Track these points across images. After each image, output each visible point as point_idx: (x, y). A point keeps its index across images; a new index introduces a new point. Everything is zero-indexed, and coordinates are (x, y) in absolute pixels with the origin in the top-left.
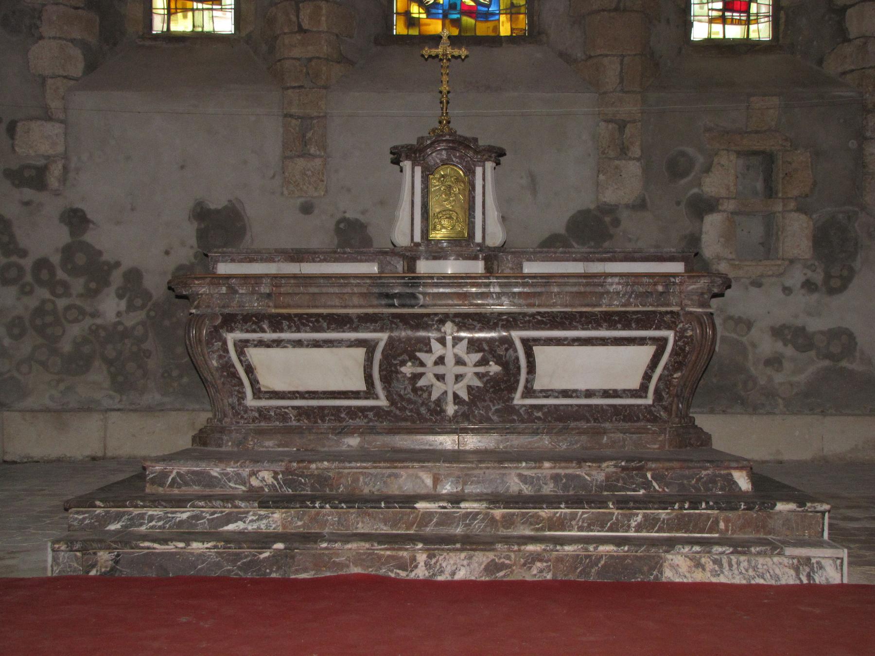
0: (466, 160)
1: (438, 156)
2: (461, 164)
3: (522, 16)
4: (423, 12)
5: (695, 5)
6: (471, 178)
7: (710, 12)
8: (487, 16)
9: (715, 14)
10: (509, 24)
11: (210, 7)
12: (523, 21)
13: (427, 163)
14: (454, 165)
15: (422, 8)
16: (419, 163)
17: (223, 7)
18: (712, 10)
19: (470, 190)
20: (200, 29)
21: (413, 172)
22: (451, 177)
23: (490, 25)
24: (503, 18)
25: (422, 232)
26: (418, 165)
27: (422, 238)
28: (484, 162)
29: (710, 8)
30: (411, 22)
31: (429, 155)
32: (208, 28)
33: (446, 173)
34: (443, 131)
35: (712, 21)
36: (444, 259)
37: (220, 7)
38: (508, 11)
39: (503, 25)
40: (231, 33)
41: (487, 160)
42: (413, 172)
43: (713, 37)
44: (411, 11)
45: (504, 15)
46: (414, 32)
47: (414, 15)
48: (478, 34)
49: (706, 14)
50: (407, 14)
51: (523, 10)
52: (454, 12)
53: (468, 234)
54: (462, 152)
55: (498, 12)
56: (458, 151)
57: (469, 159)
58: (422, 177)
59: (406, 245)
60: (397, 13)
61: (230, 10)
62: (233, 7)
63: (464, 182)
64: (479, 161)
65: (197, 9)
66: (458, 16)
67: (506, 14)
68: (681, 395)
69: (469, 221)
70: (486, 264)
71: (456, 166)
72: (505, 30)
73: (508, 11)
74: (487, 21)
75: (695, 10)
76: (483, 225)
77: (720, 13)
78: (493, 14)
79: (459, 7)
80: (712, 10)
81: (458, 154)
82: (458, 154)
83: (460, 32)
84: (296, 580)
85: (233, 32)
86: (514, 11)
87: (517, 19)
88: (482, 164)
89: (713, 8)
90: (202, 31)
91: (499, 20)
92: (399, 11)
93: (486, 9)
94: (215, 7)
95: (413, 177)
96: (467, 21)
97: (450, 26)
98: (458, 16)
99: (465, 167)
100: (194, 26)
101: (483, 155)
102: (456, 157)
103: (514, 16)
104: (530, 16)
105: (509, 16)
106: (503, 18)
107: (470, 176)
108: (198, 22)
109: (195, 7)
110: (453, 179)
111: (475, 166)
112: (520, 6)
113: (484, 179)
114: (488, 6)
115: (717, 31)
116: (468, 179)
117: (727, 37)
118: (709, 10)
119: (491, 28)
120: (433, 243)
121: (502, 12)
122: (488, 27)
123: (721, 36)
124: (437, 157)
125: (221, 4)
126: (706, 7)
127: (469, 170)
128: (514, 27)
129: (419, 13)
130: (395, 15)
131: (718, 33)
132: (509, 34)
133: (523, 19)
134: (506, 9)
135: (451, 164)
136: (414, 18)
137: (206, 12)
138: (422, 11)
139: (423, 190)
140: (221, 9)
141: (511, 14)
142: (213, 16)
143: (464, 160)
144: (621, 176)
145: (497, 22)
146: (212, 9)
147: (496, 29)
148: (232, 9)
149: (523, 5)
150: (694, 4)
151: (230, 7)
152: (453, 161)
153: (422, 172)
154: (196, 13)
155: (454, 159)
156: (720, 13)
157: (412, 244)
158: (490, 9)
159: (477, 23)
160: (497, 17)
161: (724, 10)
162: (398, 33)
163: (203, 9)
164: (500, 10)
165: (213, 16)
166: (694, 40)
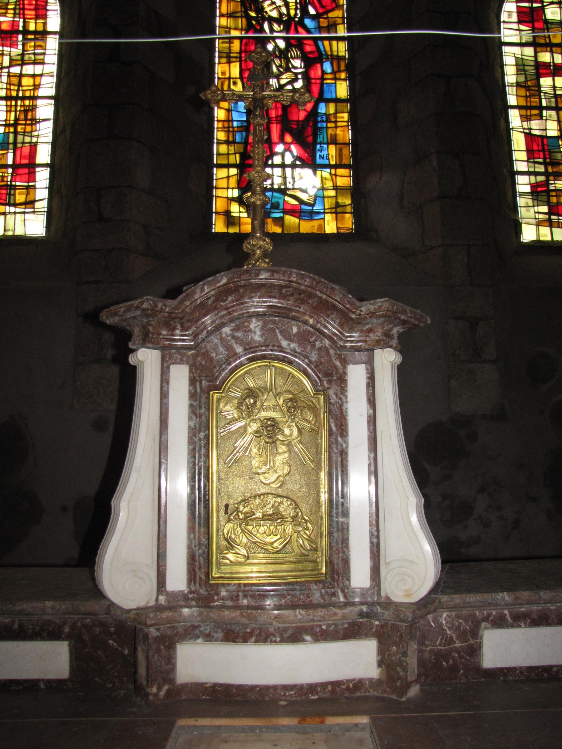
0: (318, 344)
1: (239, 334)
2: (304, 356)
3: (348, 216)
4: (244, 210)
5: (522, 208)
6: (333, 399)
7: (537, 215)
8: (311, 215)
9: (541, 216)
10: (335, 223)
11: (23, 210)
12: (348, 222)
13: (206, 355)
14: (283, 360)
15: (243, 207)
16: (182, 355)
17: (36, 210)
18: (538, 213)
19: (330, 430)
20: (11, 233)
21: (165, 380)
22: (276, 395)
23: (315, 224)
24: (328, 217)
25: (192, 558)
26: (181, 362)
27: (192, 576)
28: (371, 351)
29: (536, 211)
30: (230, 220)
31: (210, 334)
32: (19, 232)
33: (259, 382)
34: (291, 503)
35: (539, 224)
36: (257, 641)
37: (32, 210)
38: (334, 210)
39: (328, 224)
40: (42, 235)
41: (383, 344)
42: (165, 380)
43: (542, 239)
44: (232, 211)
45: (330, 214)
46: (233, 230)
47: (233, 214)
48: (302, 231)
49: (533, 217)
50: (227, 213)
51: (349, 209)
52: (277, 211)
53: (330, 563)
54: (306, 323)
55: (322, 211)
56: (294, 318)
57: (327, 342)
58: (193, 396)
59: (142, 604)
60: (217, 213)
61: (43, 213)
62: (46, 209)
63: (314, 410)
64: (358, 349)
65: (10, 213)
66: (281, 215)
67: (331, 213)
68: (293, 394)
69: (330, 525)
70: (381, 652)
71: (290, 363)
72: (330, 227)
73: (334, 210)
74: (311, 219)
75: (522, 212)
76: (372, 534)
77: (547, 217)
78: (318, 213)
79: (281, 207)
80: (538, 213)
81: (295, 330)
82: (295, 330)
83: (283, 230)
84: (306, 272)
85: (44, 235)
86: (339, 210)
87: (343, 218)
88: (363, 356)
89: (540, 211)
90: (13, 235)
91: (324, 219)
92: (219, 210)
93: (310, 208)
94: (27, 210)
95: (164, 395)
96: (290, 220)
97: (272, 225)
98: (281, 215)
99: (317, 366)
100: (5, 230)
101: (370, 330)
102: (289, 338)
103: (339, 215)
104: (356, 213)
105: (334, 215)
106: (328, 217)
107: (331, 392)
108: (10, 226)
109: (7, 211)
110: (281, 402)
111: (345, 362)
112: (346, 205)
113: (372, 401)
114: (313, 205)
115: (545, 234)
116: (328, 400)
117: (555, 239)
118: (536, 213)
119: (316, 227)
120: (223, 593)
121: (327, 211)
122: (314, 226)
123: (549, 238)
124: (233, 337)
125: (34, 208)
126: (532, 209)
127: (328, 375)
128: (340, 226)
129: (240, 212)
130: (214, 214)
131: (546, 235)
132: (335, 231)
133: (349, 218)
134: (331, 208)
135: (277, 358)
136: (234, 217)
137: (18, 216)
138: (242, 210)
139: (193, 433)
140: (34, 212)
141: (336, 213)
142: (25, 220)
143: (313, 346)
144: (475, 381)
145: (322, 221)
146: (24, 213)
147: (322, 227)
148: (44, 212)
149: (349, 205)
150: (520, 207)
151: (43, 210)
152: (282, 350)
153: (192, 382)
154: (8, 217)
155: (284, 343)
156: (547, 217)
157: (162, 598)
158: (314, 208)
159: (301, 222)
160: (322, 216)
161: (550, 213)
162: (216, 231)
163: (15, 213)
164: (324, 209)
165: (25, 220)
166: (524, 241)
